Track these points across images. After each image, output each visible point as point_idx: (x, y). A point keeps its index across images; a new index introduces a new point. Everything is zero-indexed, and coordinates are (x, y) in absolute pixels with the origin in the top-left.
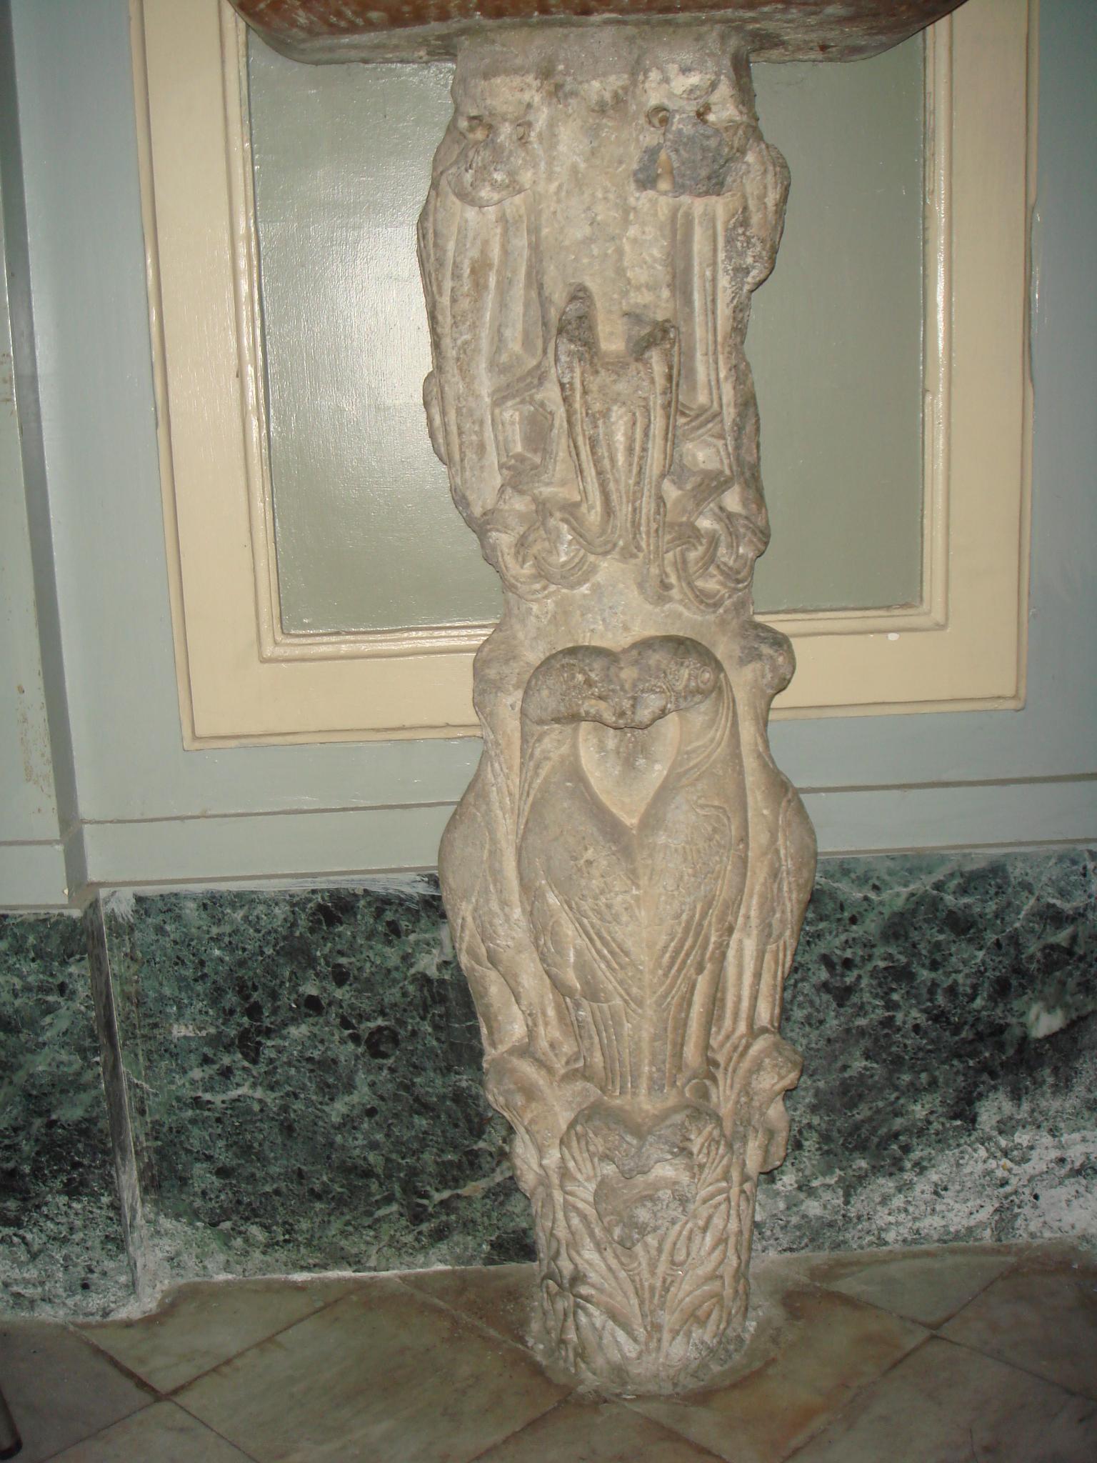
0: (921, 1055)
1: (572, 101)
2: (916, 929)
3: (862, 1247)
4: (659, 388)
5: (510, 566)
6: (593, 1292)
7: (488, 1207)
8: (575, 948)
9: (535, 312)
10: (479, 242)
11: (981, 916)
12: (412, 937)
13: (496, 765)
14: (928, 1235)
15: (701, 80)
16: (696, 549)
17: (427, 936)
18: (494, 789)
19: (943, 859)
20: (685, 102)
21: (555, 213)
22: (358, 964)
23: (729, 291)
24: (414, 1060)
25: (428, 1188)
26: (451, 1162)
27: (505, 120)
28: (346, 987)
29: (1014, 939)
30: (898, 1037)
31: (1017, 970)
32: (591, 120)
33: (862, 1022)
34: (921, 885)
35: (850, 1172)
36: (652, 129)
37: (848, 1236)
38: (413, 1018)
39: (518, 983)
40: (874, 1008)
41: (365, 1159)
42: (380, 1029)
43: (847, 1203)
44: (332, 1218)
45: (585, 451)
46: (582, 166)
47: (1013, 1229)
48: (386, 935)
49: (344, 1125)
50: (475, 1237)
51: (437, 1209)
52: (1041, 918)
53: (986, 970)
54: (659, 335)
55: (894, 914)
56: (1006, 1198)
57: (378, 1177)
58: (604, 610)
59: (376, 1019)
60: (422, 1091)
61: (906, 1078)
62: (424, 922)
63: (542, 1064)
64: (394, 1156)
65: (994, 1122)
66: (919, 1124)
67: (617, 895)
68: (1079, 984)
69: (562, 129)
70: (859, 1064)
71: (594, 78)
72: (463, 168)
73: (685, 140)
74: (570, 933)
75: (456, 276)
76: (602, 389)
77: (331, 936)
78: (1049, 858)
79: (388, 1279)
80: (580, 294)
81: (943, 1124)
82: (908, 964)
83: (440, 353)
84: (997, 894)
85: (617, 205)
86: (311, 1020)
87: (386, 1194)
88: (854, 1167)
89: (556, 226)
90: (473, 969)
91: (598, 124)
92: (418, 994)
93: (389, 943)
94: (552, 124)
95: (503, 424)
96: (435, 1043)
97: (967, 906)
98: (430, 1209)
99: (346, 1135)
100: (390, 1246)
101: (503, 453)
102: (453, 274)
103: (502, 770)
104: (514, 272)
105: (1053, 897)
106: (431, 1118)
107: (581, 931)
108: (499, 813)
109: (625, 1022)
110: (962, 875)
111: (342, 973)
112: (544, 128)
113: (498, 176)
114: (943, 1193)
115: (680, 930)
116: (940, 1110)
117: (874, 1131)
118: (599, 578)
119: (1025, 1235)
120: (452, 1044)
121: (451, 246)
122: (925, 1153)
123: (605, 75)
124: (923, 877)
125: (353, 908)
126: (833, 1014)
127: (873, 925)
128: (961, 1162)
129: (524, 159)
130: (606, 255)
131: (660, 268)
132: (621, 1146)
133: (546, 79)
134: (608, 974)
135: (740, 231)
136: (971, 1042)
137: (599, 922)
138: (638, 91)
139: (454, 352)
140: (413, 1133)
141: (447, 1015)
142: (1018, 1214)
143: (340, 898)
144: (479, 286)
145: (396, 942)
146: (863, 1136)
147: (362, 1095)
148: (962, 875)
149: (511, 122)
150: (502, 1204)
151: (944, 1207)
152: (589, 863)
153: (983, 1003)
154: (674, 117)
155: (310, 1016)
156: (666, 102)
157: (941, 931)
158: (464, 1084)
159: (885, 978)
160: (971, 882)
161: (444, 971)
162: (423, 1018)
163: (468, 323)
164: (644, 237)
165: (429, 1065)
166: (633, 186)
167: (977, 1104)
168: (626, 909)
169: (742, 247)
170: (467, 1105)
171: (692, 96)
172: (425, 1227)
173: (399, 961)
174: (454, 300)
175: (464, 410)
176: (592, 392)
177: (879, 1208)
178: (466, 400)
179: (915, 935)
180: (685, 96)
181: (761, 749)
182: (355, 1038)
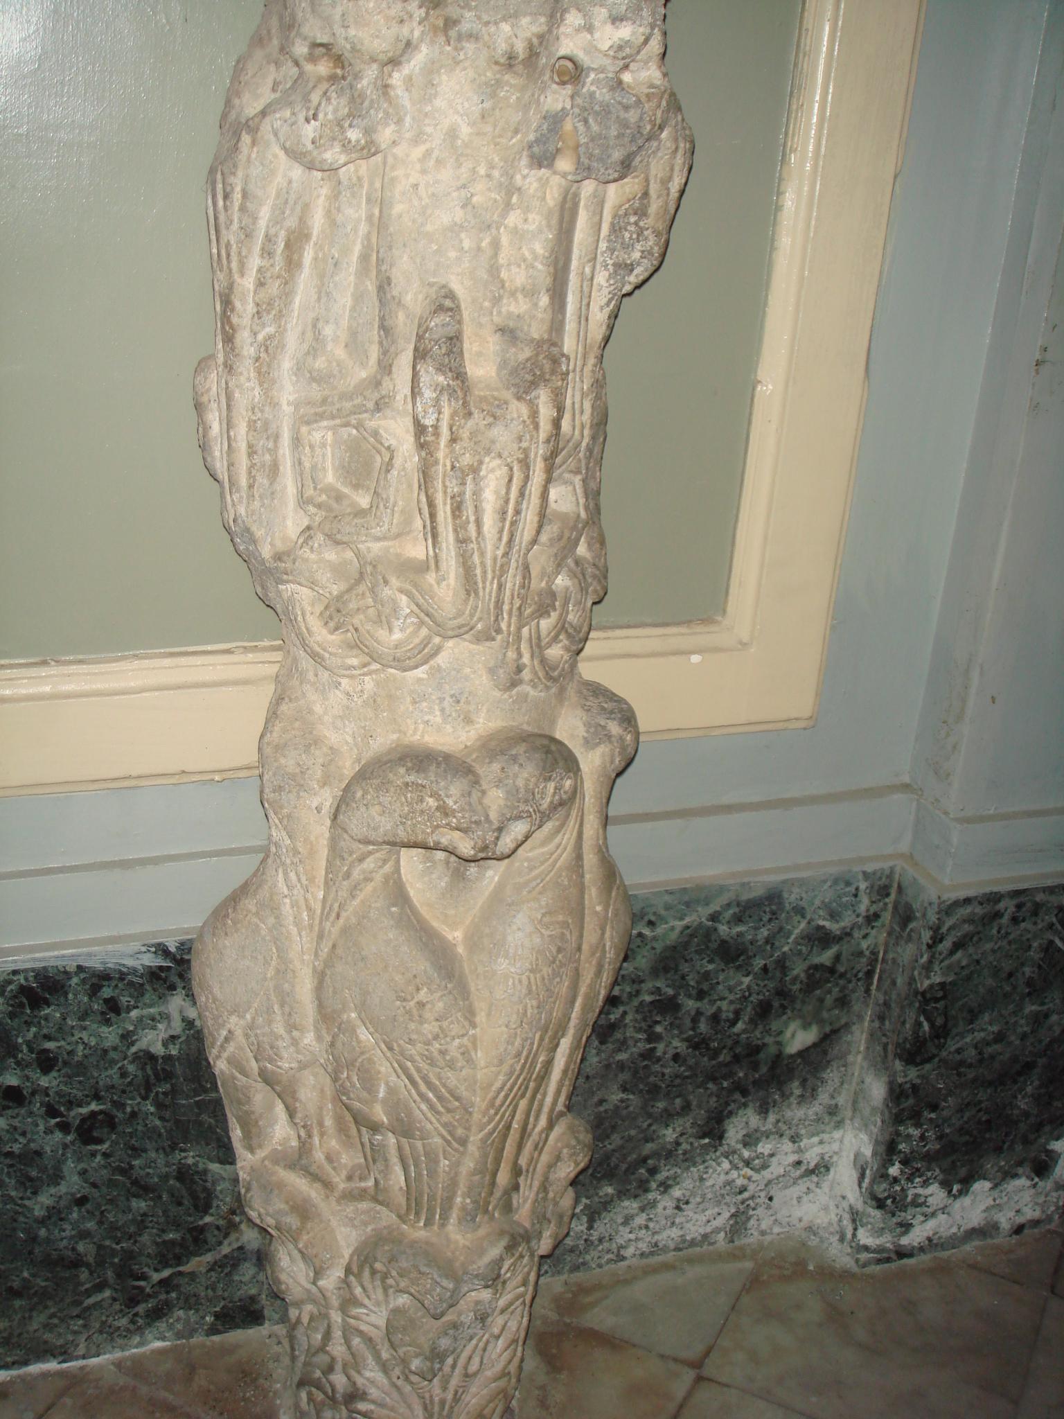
0: (678, 1081)
1: (470, 47)
2: (686, 961)
3: (600, 1266)
4: (542, 436)
5: (314, 629)
6: (372, 1407)
7: (213, 1279)
8: (387, 1084)
9: (371, 308)
10: (298, 208)
11: (752, 943)
12: (134, 1014)
13: (292, 875)
14: (665, 1246)
15: (634, 33)
16: (549, 616)
17: (152, 1010)
18: (287, 901)
19: (722, 889)
20: (609, 61)
21: (416, 186)
22: (69, 1048)
23: (605, 291)
24: (133, 1142)
25: (146, 1269)
26: (173, 1242)
28: (54, 1074)
29: (782, 964)
30: (657, 1068)
31: (781, 993)
33: (622, 1056)
34: (695, 918)
35: (596, 1199)
37: (588, 1257)
38: (133, 1099)
39: (296, 1099)
40: (636, 1042)
41: (74, 1249)
42: (93, 1114)
43: (590, 1227)
44: (34, 1314)
45: (444, 512)
46: (465, 131)
47: (746, 1229)
48: (103, 1013)
49: (49, 1217)
50: (197, 1311)
51: (157, 1289)
52: (810, 940)
53: (750, 995)
54: (547, 366)
55: (666, 948)
56: (743, 1203)
57: (88, 1265)
58: (444, 699)
59: (89, 1104)
60: (142, 1173)
61: (661, 1105)
62: (147, 998)
63: (315, 1177)
64: (107, 1243)
65: (740, 1136)
66: (669, 1147)
67: (453, 1039)
68: (836, 1000)
69: (444, 77)
70: (616, 1096)
73: (597, 108)
74: (383, 1069)
76: (473, 434)
77: (36, 1020)
78: (825, 881)
79: (101, 1367)
80: (446, 304)
81: (691, 1144)
82: (675, 997)
83: (233, 349)
84: (770, 920)
85: (501, 185)
86: (9, 1112)
87: (98, 1280)
88: (601, 1194)
89: (416, 203)
90: (234, 1078)
92: (139, 1073)
93: (108, 1022)
94: (431, 70)
95: (311, 447)
96: (158, 1123)
97: (740, 935)
98: (148, 1290)
99: (51, 1227)
100: (101, 1332)
101: (309, 483)
102: (263, 249)
103: (299, 880)
105: (824, 919)
106: (151, 1199)
107: (399, 1071)
108: (294, 930)
109: (442, 1158)
110: (738, 905)
111: (49, 1059)
114: (684, 1206)
115: (518, 1068)
116: (690, 1131)
117: (625, 1156)
118: (441, 660)
119: (756, 1233)
120: (177, 1122)
122: (672, 1172)
123: (516, 15)
124: (700, 909)
125: (63, 987)
126: (594, 1051)
127: (644, 960)
128: (705, 1176)
129: (387, 113)
130: (479, 249)
131: (540, 267)
132: (435, 1290)
133: (434, 9)
134: (429, 1115)
135: (633, 219)
136: (727, 1065)
137: (427, 1067)
140: (130, 1217)
141: (174, 1092)
142: (752, 1216)
143: (46, 977)
144: (293, 264)
145: (114, 1020)
146: (612, 1164)
147: (72, 1183)
148: (738, 905)
150: (229, 1274)
151: (683, 1219)
152: (421, 1005)
153: (744, 1027)
154: (587, 76)
155: (9, 1108)
156: (581, 56)
157: (710, 962)
158: (190, 1161)
159: (650, 1011)
160: (746, 910)
161: (171, 1046)
162: (145, 1098)
163: (274, 312)
164: (526, 227)
165: (149, 1145)
166: (524, 161)
167: (727, 1122)
168: (463, 1054)
169: (631, 238)
170: (193, 1182)
172: (141, 1308)
173: (117, 1041)
174: (261, 284)
176: (461, 440)
177: (621, 1228)
178: (262, 411)
179: (685, 968)
180: (611, 53)
181: (601, 842)
182: (64, 1127)
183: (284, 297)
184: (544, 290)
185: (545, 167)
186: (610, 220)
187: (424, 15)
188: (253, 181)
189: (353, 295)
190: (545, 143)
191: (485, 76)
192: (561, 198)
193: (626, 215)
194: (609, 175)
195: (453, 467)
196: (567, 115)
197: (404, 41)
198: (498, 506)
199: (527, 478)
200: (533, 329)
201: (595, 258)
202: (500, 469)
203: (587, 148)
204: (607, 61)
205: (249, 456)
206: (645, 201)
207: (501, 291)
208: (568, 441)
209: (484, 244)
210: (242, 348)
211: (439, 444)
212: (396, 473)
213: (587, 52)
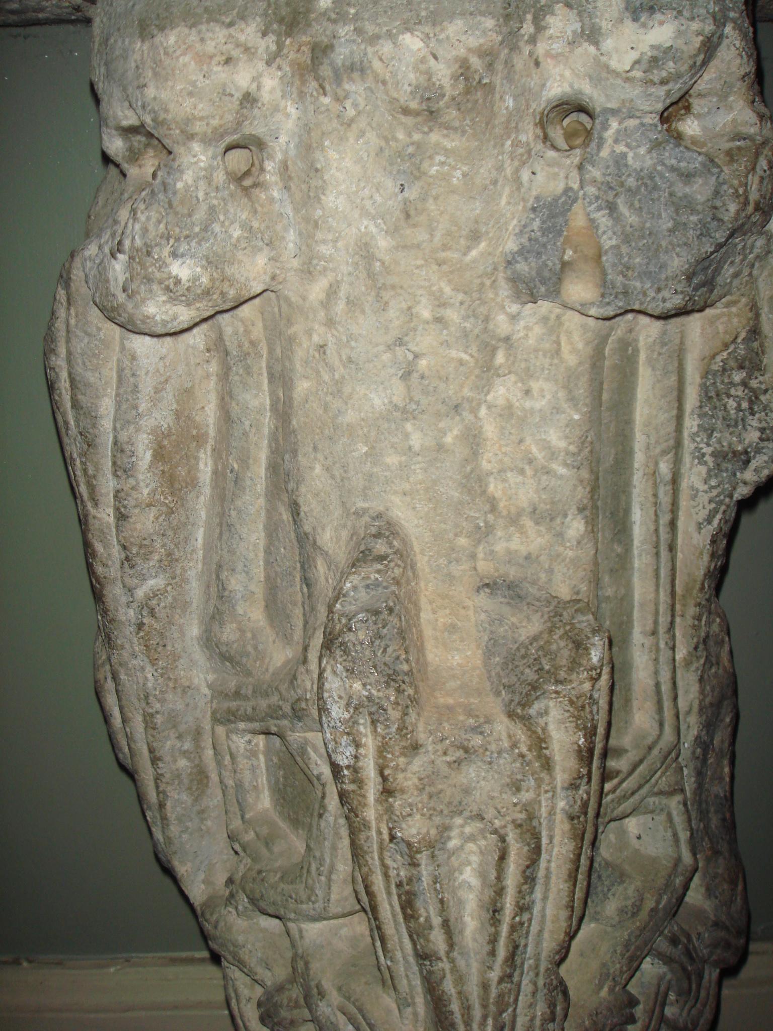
9: (287, 553)
10: (169, 396)
15: (679, 33)
20: (637, 91)
21: (322, 348)
23: (704, 498)
27: (191, 137)
32: (401, 136)
36: (551, 154)
46: (383, 243)
71: (408, 28)
72: (107, 250)
73: (631, 182)
75: (122, 470)
85: (465, 334)
91: (418, 145)
104: (244, 461)
112: (292, 152)
113: (182, 270)
121: (106, 407)
123: (436, 19)
130: (440, 447)
131: (562, 471)
133: (289, 34)
135: (738, 377)
138: (519, 62)
139: (131, 612)
149: (206, 141)
154: (605, 126)
156: (588, 91)
163: (156, 557)
164: (528, 404)
166: (505, 290)
169: (739, 409)
171: (656, 76)
174: (121, 517)
175: (159, 719)
180: (637, 74)
183: (170, 533)
184: (574, 510)
185: (545, 297)
186: (698, 380)
187: (274, 48)
188: (80, 361)
189: (266, 528)
190: (539, 254)
191: (396, 139)
192: (589, 350)
193: (724, 370)
194: (664, 300)
195: (392, 838)
196: (575, 201)
197: (238, 95)
198: (486, 898)
199: (536, 851)
200: (558, 577)
201: (678, 444)
202: (485, 838)
203: (620, 256)
204: (634, 92)
205: (153, 764)
206: (756, 345)
207: (490, 517)
208: (650, 748)
209: (449, 439)
210: (117, 611)
211: (364, 796)
212: (331, 819)
213: (596, 80)
